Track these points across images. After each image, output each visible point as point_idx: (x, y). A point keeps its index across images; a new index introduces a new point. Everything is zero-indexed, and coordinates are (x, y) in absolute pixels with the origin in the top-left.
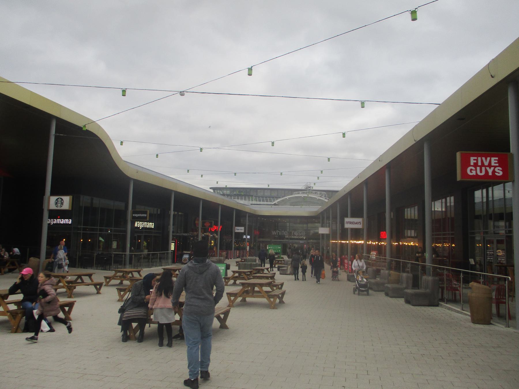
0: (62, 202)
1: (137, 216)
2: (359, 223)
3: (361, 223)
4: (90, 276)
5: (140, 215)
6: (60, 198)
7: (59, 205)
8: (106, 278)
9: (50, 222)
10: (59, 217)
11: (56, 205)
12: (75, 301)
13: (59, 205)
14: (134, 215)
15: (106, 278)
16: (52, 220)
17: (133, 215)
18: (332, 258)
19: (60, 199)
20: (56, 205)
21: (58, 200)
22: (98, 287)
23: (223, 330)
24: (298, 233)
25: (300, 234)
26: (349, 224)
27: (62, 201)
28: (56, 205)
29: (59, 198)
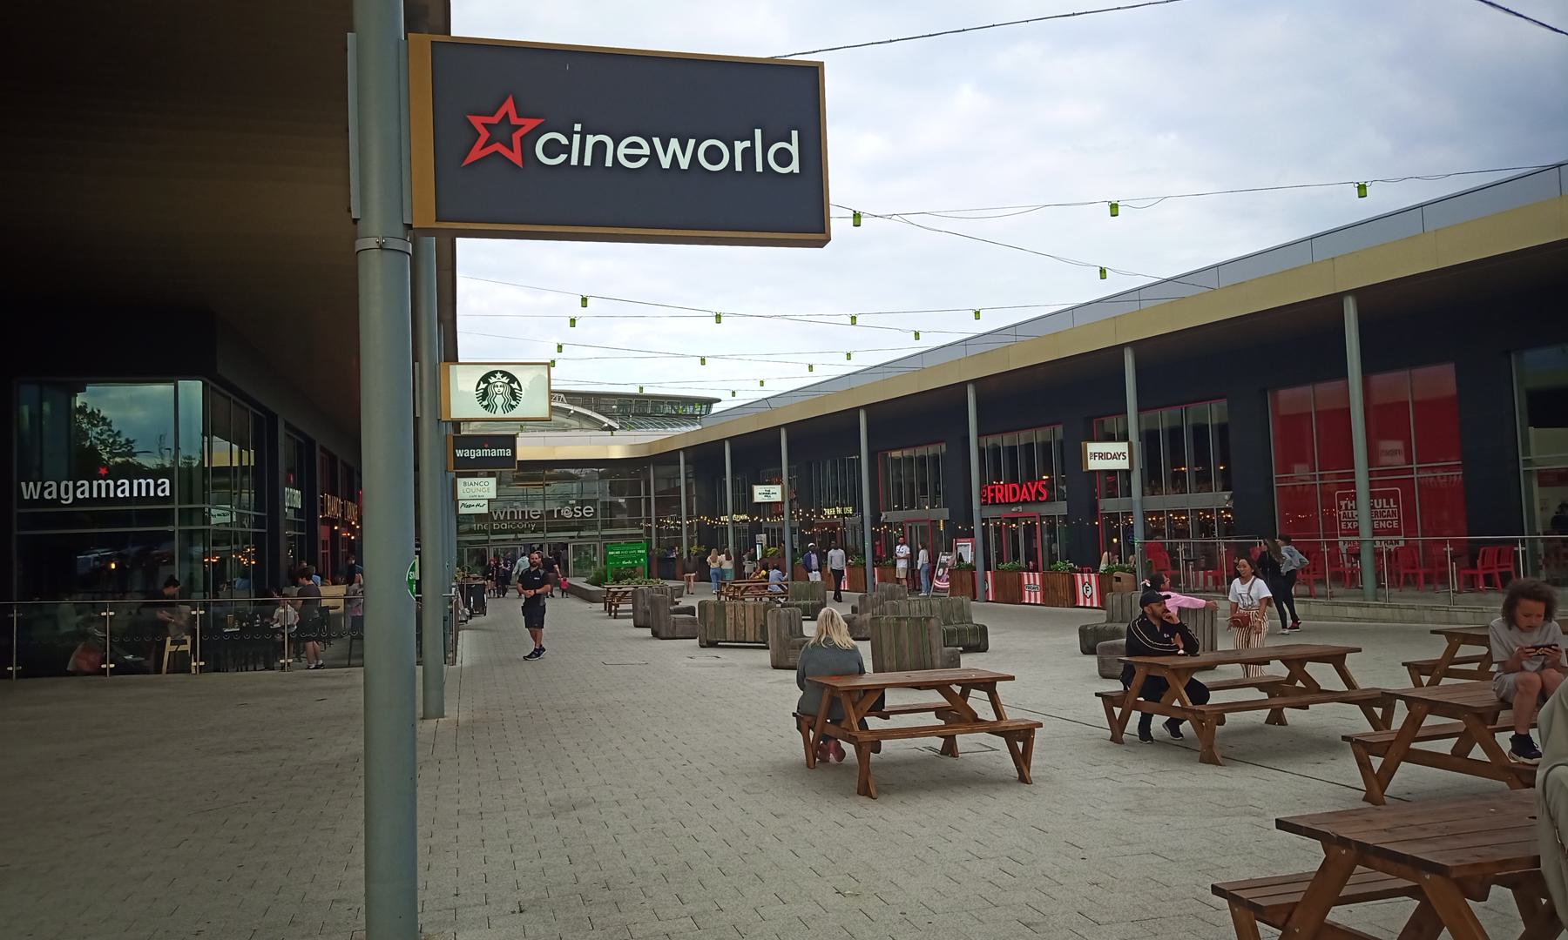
1: (473, 457)
2: (1122, 457)
3: (1127, 455)
5: (485, 452)
6: (501, 372)
7: (499, 400)
8: (1416, 669)
9: (54, 496)
10: (486, 446)
11: (485, 403)
14: (459, 453)
15: (1416, 669)
16: (67, 486)
17: (455, 454)
18: (497, 565)
19: (499, 375)
20: (485, 403)
21: (492, 380)
22: (1379, 711)
23: (1022, 784)
24: (573, 510)
25: (578, 514)
26: (1097, 458)
27: (515, 386)
28: (484, 400)
29: (496, 372)
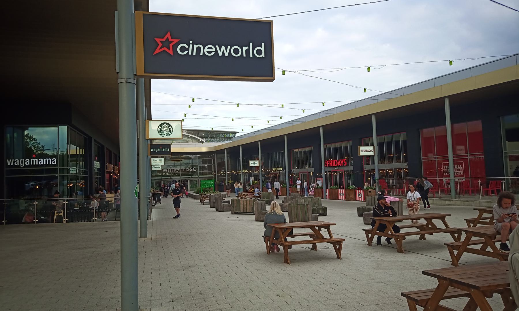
0: (170, 129)
1: (157, 151)
2: (371, 151)
3: (373, 150)
4: (442, 218)
5: (161, 150)
6: (166, 123)
7: (165, 132)
9: (18, 164)
10: (161, 147)
11: (161, 133)
12: (509, 253)
13: (165, 132)
14: (152, 150)
16: (22, 161)
17: (151, 150)
19: (165, 124)
20: (161, 133)
21: (163, 126)
23: (338, 260)
24: (190, 169)
25: (191, 170)
26: (363, 152)
28: (160, 132)
29: (164, 123)
